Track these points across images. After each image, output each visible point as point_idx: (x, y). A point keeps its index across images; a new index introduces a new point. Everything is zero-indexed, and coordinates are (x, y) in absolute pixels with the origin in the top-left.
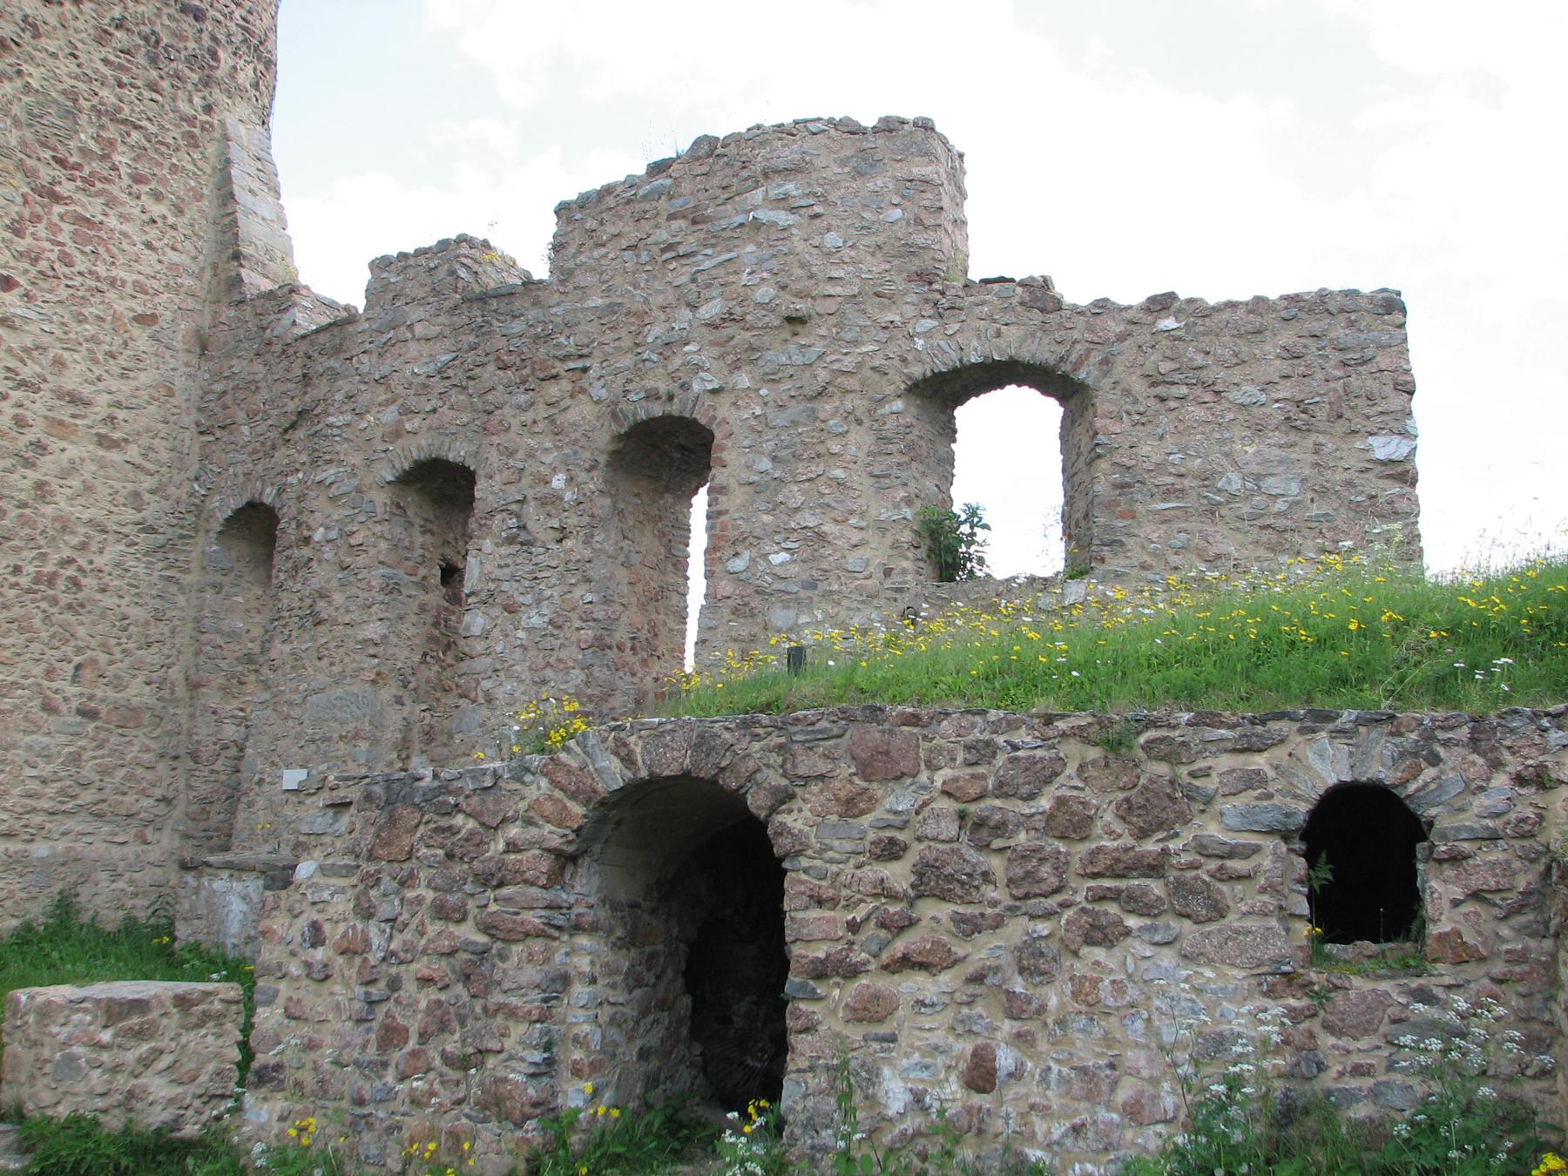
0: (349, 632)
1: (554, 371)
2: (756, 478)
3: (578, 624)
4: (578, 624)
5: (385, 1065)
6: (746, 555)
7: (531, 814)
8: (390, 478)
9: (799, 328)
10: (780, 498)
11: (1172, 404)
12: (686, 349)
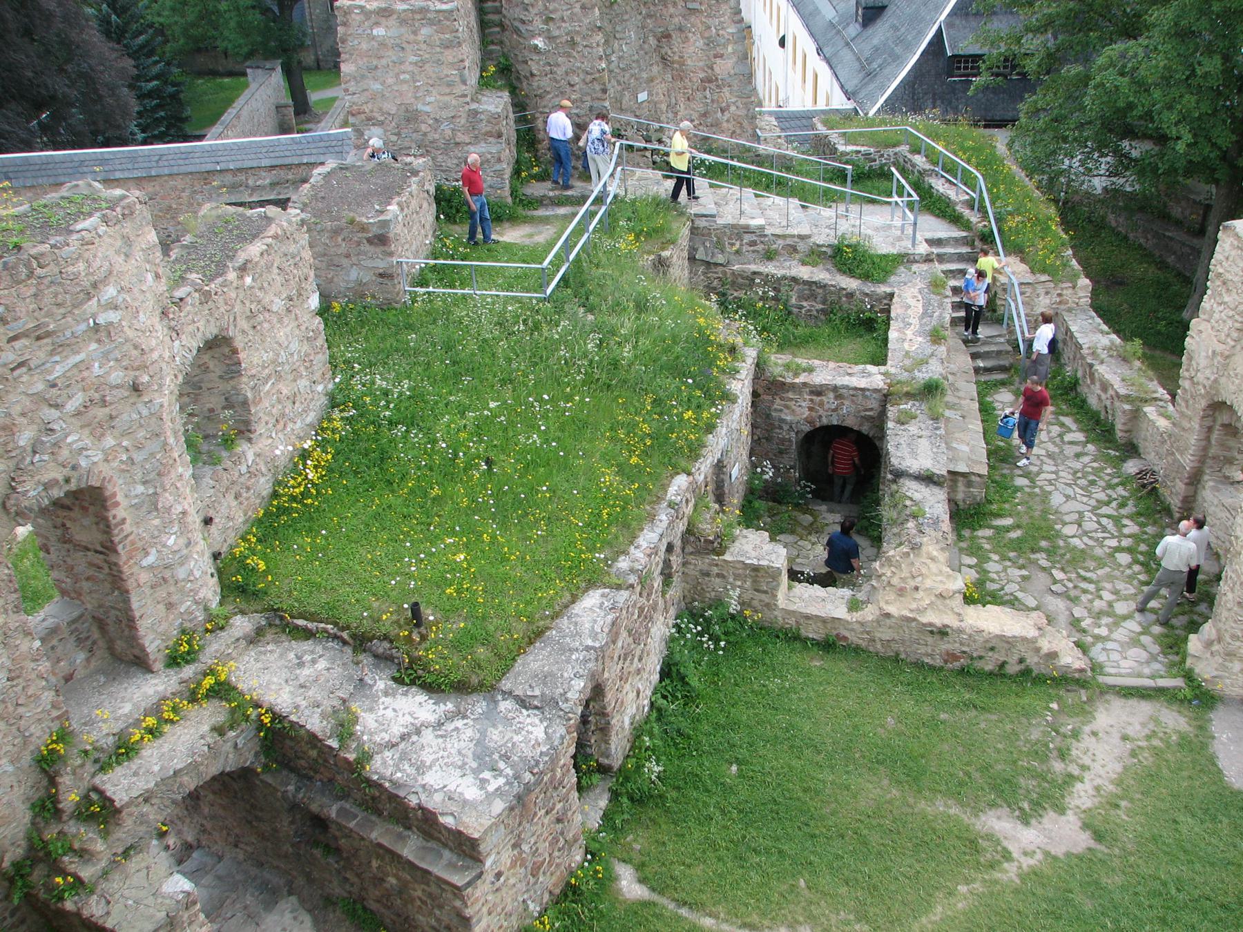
6: (153, 551)
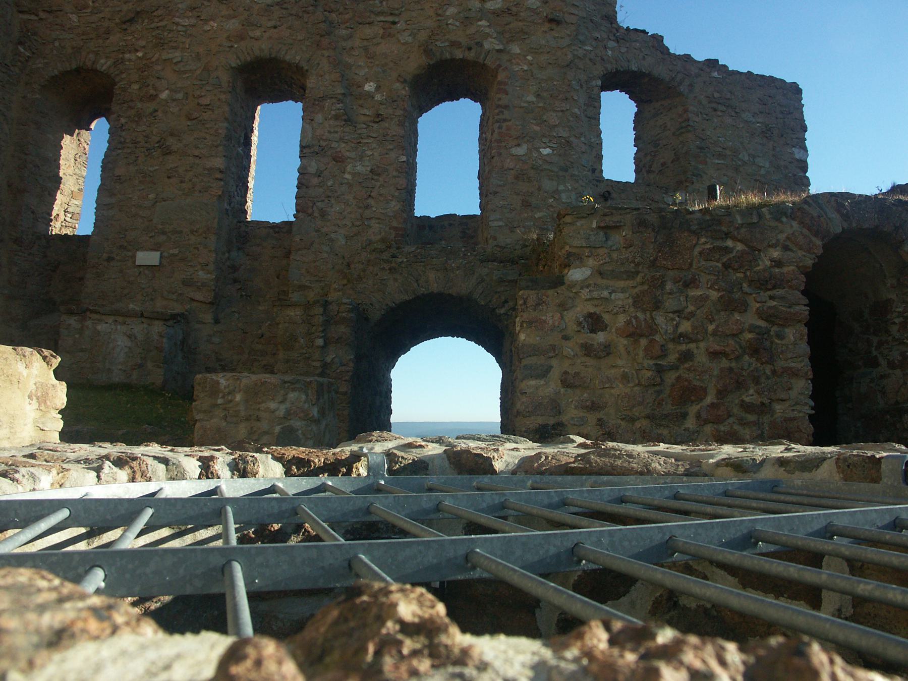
0: (197, 161)
1: (369, 20)
2: (525, 105)
3: (395, 174)
4: (395, 174)
5: (684, 416)
6: (525, 146)
7: (788, 243)
8: (233, 65)
9: (554, 26)
10: (545, 118)
11: (720, 114)
12: (480, 23)
